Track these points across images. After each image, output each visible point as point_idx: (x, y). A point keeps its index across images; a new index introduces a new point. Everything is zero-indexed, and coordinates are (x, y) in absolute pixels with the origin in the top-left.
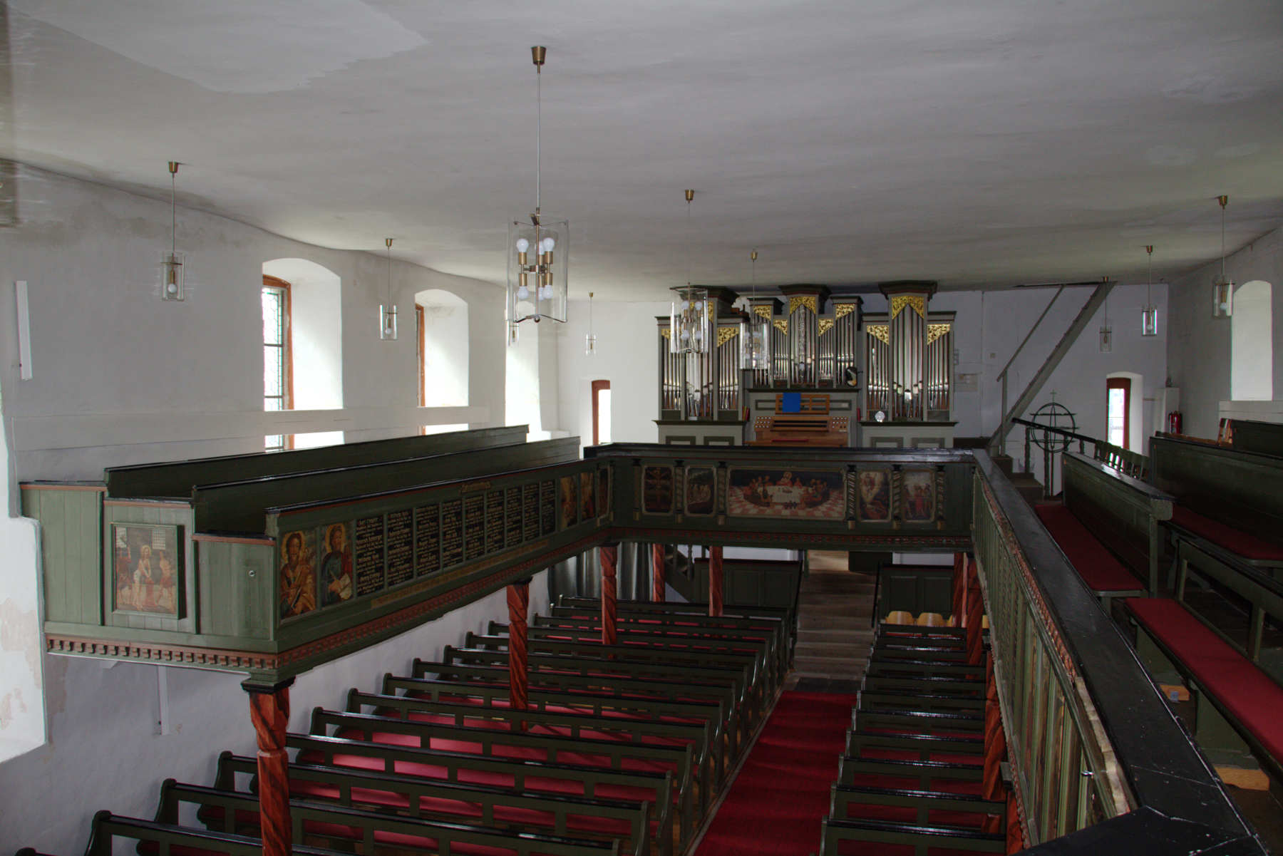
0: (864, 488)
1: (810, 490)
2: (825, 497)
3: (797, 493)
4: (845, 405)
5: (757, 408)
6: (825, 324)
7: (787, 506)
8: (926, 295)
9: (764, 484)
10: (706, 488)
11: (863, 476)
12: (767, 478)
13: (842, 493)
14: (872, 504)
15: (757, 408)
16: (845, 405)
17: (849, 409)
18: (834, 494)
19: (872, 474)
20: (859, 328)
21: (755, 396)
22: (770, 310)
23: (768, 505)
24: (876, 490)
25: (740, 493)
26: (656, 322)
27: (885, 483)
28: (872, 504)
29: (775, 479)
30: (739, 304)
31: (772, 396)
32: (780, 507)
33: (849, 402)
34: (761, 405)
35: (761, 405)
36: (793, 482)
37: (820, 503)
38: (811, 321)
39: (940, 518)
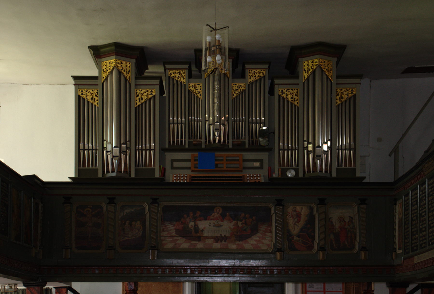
0: (291, 222)
1: (240, 224)
2: (254, 230)
3: (227, 226)
4: (257, 164)
5: (173, 168)
6: (238, 87)
7: (217, 239)
8: (335, 59)
9: (195, 219)
10: (138, 224)
11: (290, 210)
12: (198, 213)
13: (270, 226)
14: (298, 236)
15: (173, 168)
16: (257, 164)
17: (261, 167)
18: (263, 228)
19: (298, 208)
20: (271, 92)
21: (170, 156)
22: (185, 74)
23: (199, 239)
24: (302, 223)
25: (171, 228)
26: (72, 81)
27: (311, 219)
28: (298, 236)
29: (206, 213)
30: (153, 69)
31: (187, 155)
32: (210, 241)
33: (261, 161)
34: (176, 164)
35: (176, 164)
36: (223, 217)
37: (249, 236)
38: (223, 80)
39: (363, 249)
